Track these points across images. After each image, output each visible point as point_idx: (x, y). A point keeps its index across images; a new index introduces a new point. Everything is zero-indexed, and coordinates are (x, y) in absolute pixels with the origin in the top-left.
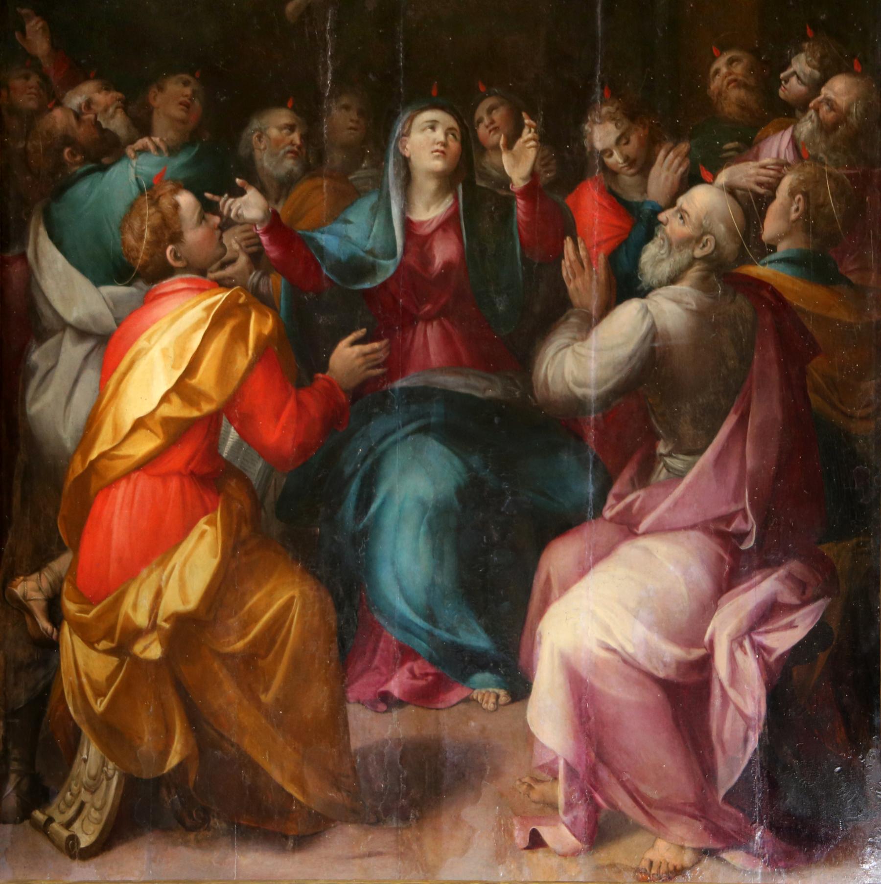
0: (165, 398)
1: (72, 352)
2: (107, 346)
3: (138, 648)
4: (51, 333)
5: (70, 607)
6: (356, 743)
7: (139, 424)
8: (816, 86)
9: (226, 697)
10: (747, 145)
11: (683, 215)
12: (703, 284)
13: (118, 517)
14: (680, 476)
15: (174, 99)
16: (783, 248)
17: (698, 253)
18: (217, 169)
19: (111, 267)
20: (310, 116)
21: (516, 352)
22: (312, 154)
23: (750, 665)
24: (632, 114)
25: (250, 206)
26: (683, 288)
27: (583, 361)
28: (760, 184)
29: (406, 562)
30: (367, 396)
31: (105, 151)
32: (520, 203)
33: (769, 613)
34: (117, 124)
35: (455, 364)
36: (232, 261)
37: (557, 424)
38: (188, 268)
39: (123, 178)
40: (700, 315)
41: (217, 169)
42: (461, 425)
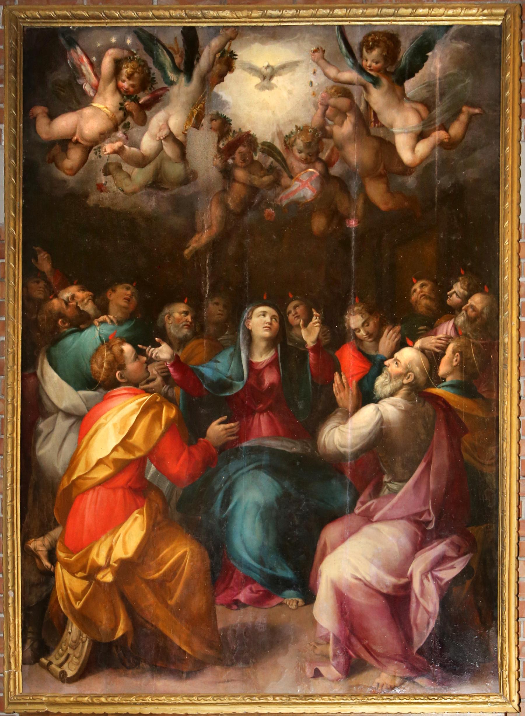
0: (115, 449)
2: (82, 422)
3: (99, 576)
5: (61, 554)
6: (220, 626)
7: (100, 462)
8: (466, 299)
9: (149, 603)
10: (431, 328)
11: (397, 362)
12: (408, 397)
13: (88, 509)
14: (395, 492)
15: (121, 296)
17: (405, 381)
18: (144, 330)
20: (197, 307)
21: (311, 431)
22: (198, 327)
23: (431, 586)
24: (370, 311)
25: (164, 352)
26: (397, 398)
27: (345, 434)
28: (437, 347)
29: (248, 535)
30: (228, 450)
31: (81, 321)
33: (442, 561)
34: (89, 308)
35: (276, 435)
37: (332, 466)
38: (128, 383)
39: (91, 337)
40: (406, 412)
42: (279, 466)
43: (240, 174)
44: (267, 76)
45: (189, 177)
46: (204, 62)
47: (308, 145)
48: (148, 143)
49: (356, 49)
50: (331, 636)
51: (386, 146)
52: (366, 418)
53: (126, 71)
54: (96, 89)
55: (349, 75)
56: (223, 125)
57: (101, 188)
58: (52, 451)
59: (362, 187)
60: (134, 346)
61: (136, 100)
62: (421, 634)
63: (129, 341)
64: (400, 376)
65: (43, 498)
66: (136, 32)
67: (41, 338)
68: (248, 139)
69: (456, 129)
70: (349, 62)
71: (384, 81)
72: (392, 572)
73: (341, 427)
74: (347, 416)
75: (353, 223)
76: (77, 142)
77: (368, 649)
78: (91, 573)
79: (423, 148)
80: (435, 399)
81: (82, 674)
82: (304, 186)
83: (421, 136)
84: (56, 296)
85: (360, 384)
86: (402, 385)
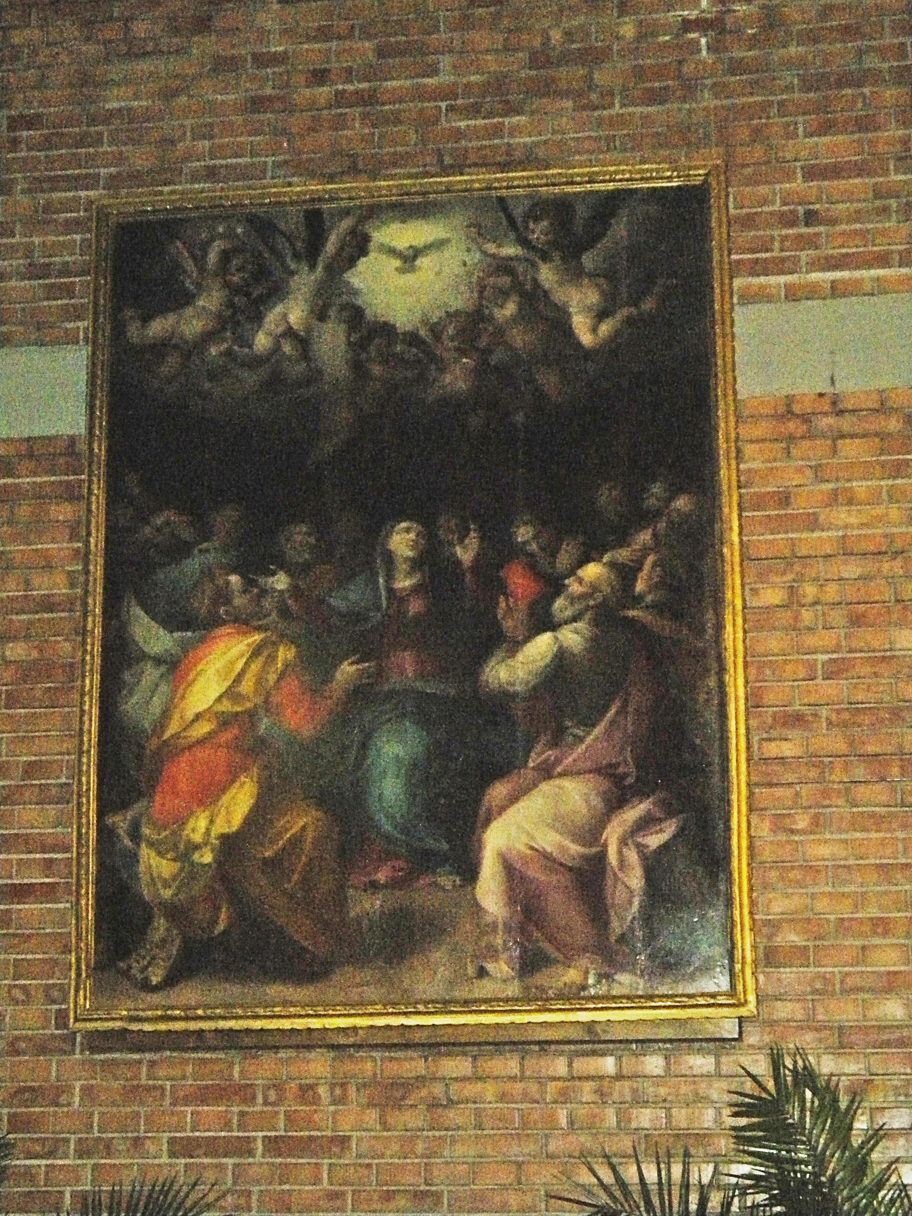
0: (219, 699)
1: (151, 673)
2: (175, 667)
3: (196, 857)
4: (138, 660)
5: (146, 831)
7: (198, 717)
9: (259, 885)
10: (622, 539)
11: (580, 581)
12: (595, 622)
13: (182, 773)
14: (581, 740)
15: (225, 519)
16: (649, 598)
17: (592, 603)
19: (177, 619)
22: (324, 551)
23: (633, 856)
24: (542, 523)
25: (281, 582)
26: (579, 625)
28: (632, 561)
29: (389, 791)
30: (359, 694)
31: (179, 550)
32: (468, 577)
33: (645, 824)
36: (269, 615)
37: (499, 705)
38: (236, 620)
39: (193, 564)
40: (594, 639)
41: (254, 561)
42: (423, 710)
43: (376, 370)
44: (409, 259)
45: (314, 376)
46: (331, 246)
47: (461, 332)
48: (262, 341)
49: (519, 220)
50: (500, 920)
51: (560, 324)
52: (542, 646)
53: (235, 262)
54: (199, 286)
55: (511, 250)
56: (355, 316)
57: (205, 396)
58: (142, 701)
59: (531, 381)
60: (243, 576)
61: (248, 295)
62: (622, 919)
63: (234, 570)
64: (582, 597)
65: (128, 765)
66: (247, 220)
67: (130, 574)
68: (386, 329)
69: (648, 305)
70: (512, 235)
71: (556, 256)
72: (577, 838)
73: (509, 661)
74: (516, 646)
75: (519, 418)
76: (176, 347)
77: (551, 939)
78: (186, 854)
79: (605, 328)
80: (631, 623)
81: (170, 982)
82: (456, 378)
83: (602, 315)
84: (148, 523)
85: (532, 606)
86: (588, 608)
